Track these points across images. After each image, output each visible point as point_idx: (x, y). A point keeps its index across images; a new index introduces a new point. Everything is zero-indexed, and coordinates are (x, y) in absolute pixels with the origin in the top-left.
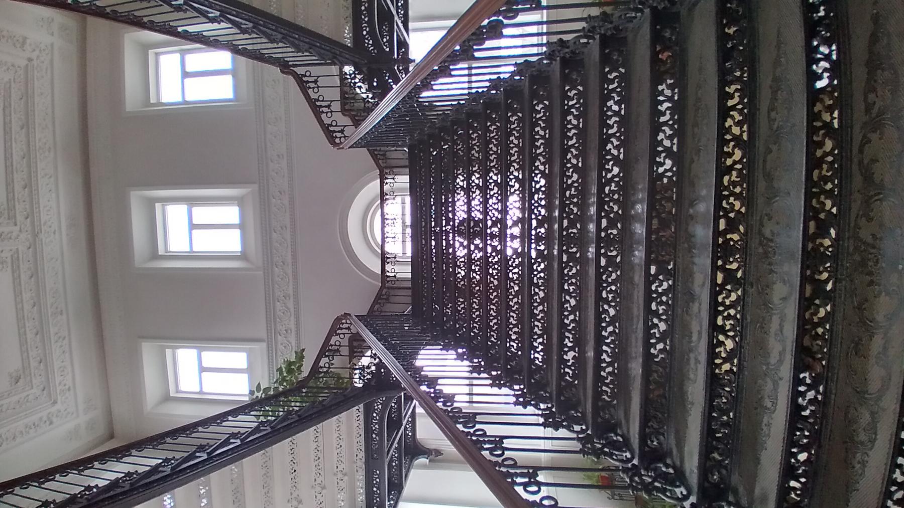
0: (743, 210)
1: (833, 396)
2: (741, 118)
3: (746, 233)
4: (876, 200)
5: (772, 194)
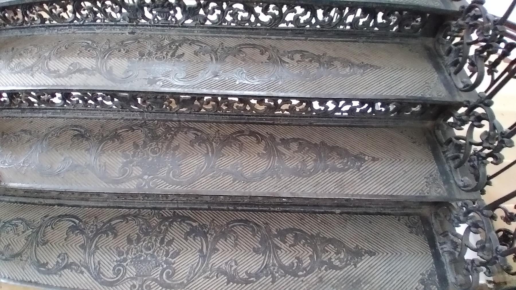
0: (208, 23)
1: (41, 115)
2: (302, 21)
3: (183, 26)
4: (211, 58)
5: (220, 55)
